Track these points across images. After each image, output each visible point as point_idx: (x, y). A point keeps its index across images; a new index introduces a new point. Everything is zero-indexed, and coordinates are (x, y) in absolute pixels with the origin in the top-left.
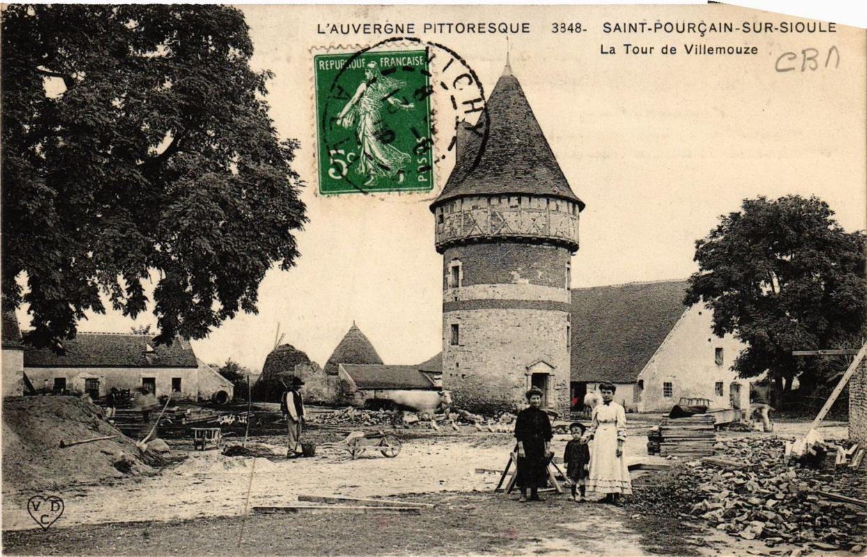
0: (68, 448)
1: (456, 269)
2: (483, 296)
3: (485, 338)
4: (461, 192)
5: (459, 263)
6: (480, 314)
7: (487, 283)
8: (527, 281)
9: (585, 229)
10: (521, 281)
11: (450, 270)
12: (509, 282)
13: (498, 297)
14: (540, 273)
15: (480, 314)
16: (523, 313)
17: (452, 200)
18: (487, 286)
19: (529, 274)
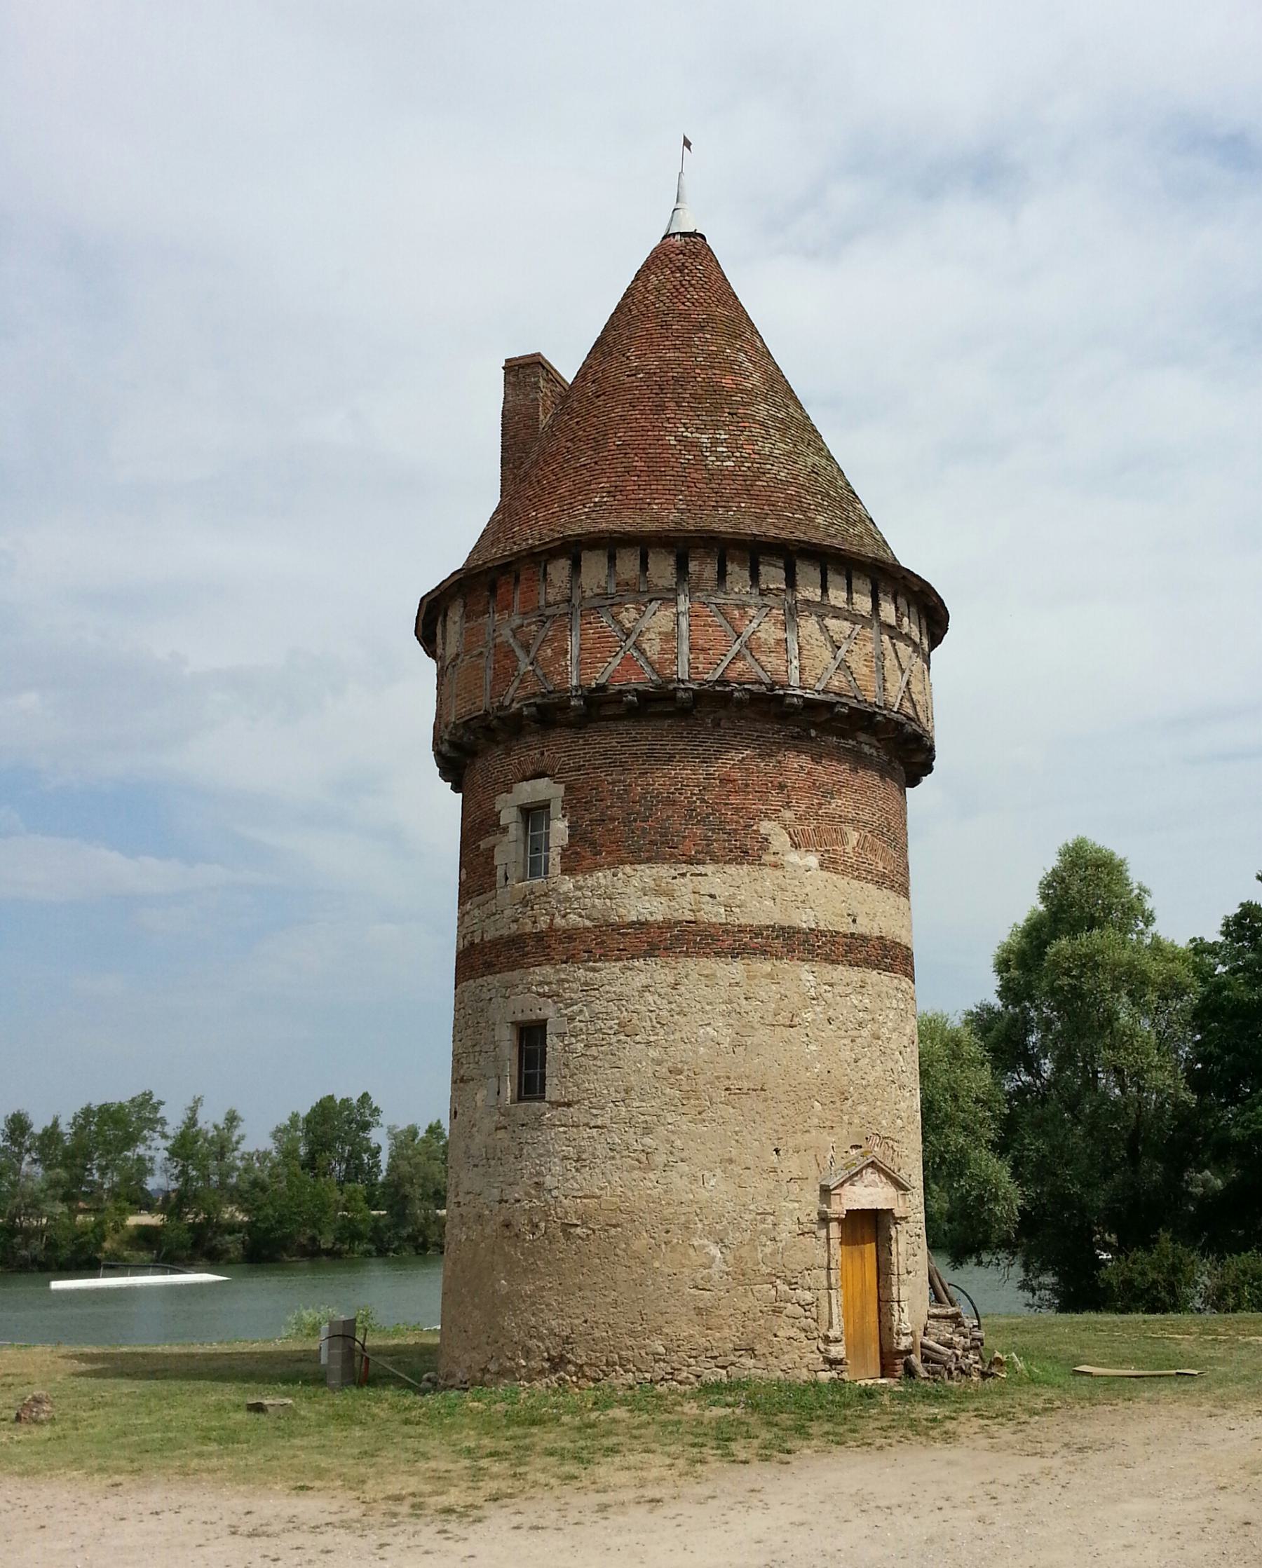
0: (768, 870)
1: (534, 814)
2: (655, 910)
3: (664, 1070)
4: (581, 523)
5: (542, 789)
6: (641, 980)
7: (673, 859)
8: (813, 860)
9: (955, 689)
10: (793, 857)
11: (509, 816)
12: (757, 860)
13: (713, 914)
14: (854, 837)
15: (642, 980)
16: (806, 975)
17: (539, 557)
18: (664, 871)
19: (817, 837)
